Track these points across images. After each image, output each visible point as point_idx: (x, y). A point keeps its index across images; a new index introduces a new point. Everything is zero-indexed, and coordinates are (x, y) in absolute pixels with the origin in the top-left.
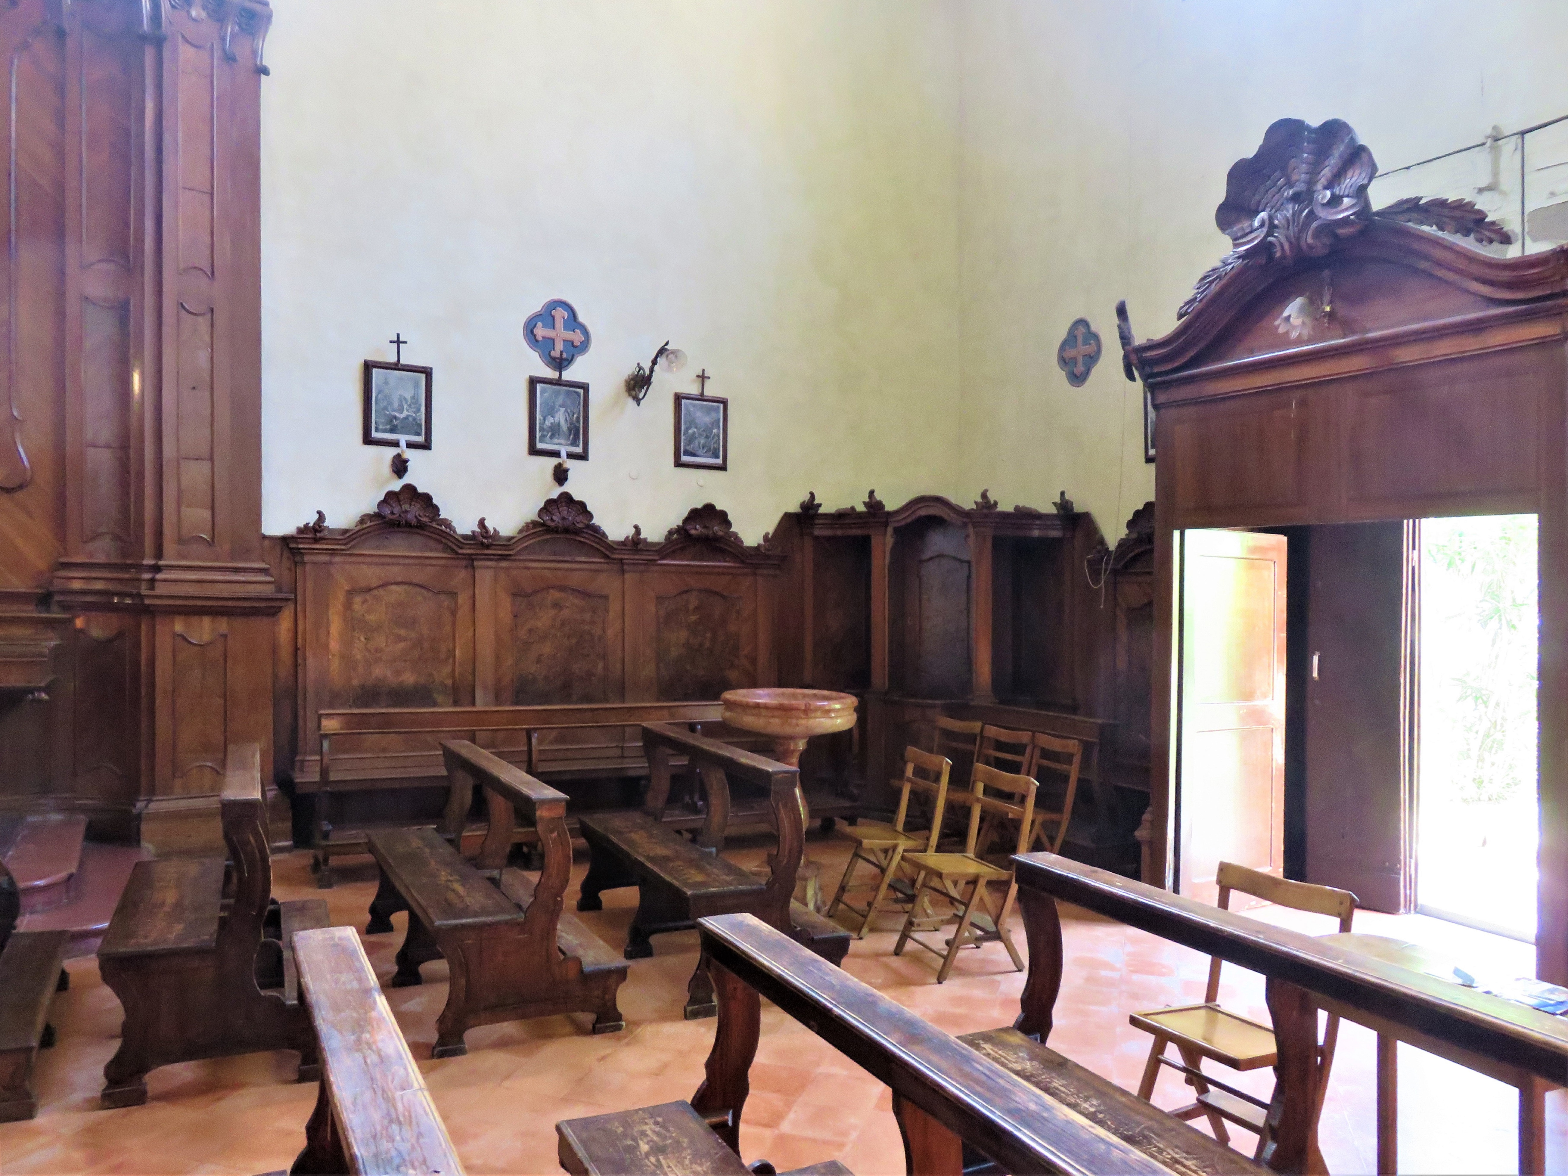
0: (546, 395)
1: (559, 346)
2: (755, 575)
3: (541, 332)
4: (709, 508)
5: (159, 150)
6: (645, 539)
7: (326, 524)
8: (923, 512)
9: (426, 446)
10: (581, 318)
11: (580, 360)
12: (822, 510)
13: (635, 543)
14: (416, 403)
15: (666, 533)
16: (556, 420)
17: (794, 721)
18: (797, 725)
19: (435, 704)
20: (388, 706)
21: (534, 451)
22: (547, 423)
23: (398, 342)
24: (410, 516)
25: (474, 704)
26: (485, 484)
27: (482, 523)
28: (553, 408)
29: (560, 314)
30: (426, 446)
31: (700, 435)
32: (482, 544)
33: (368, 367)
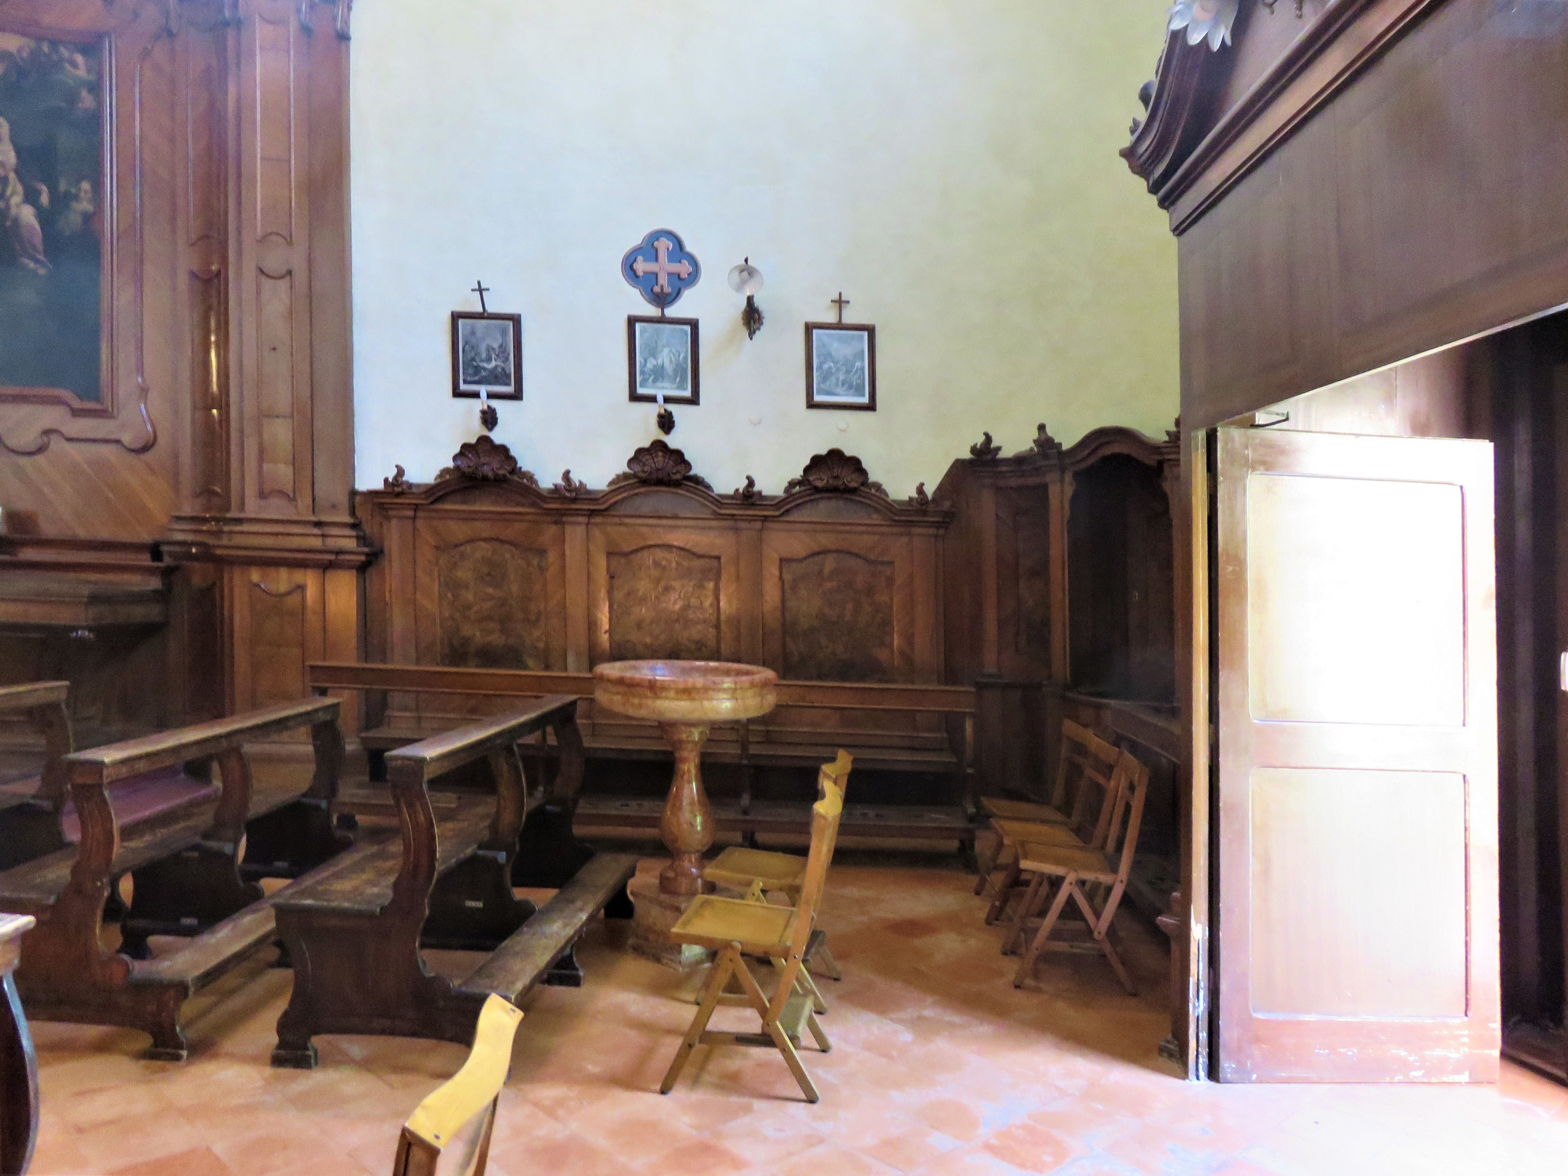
0: (647, 335)
1: (663, 280)
2: (909, 534)
3: (641, 266)
4: (835, 455)
5: (239, 125)
6: (760, 493)
7: (405, 479)
8: (1108, 451)
9: (517, 396)
10: (689, 247)
11: (688, 295)
12: (1002, 455)
13: (749, 497)
14: (504, 352)
15: (786, 484)
16: (660, 361)
17: (636, 701)
18: (640, 706)
19: (526, 668)
20: (477, 666)
21: (635, 397)
22: (649, 366)
23: (481, 290)
24: (486, 470)
25: (566, 670)
26: (578, 434)
27: (566, 475)
28: (655, 348)
29: (664, 245)
30: (517, 396)
31: (838, 370)
32: (566, 498)
33: (456, 317)
